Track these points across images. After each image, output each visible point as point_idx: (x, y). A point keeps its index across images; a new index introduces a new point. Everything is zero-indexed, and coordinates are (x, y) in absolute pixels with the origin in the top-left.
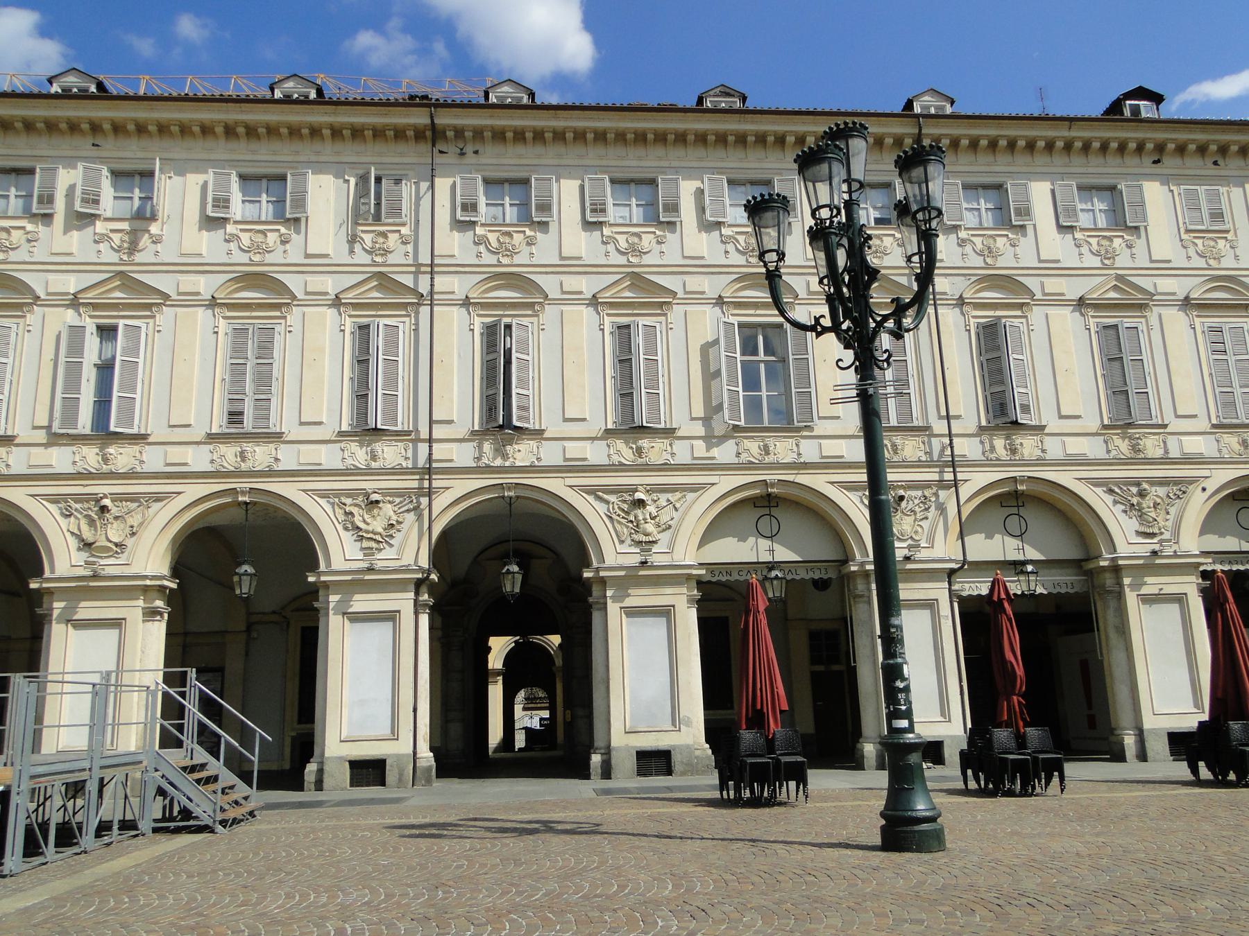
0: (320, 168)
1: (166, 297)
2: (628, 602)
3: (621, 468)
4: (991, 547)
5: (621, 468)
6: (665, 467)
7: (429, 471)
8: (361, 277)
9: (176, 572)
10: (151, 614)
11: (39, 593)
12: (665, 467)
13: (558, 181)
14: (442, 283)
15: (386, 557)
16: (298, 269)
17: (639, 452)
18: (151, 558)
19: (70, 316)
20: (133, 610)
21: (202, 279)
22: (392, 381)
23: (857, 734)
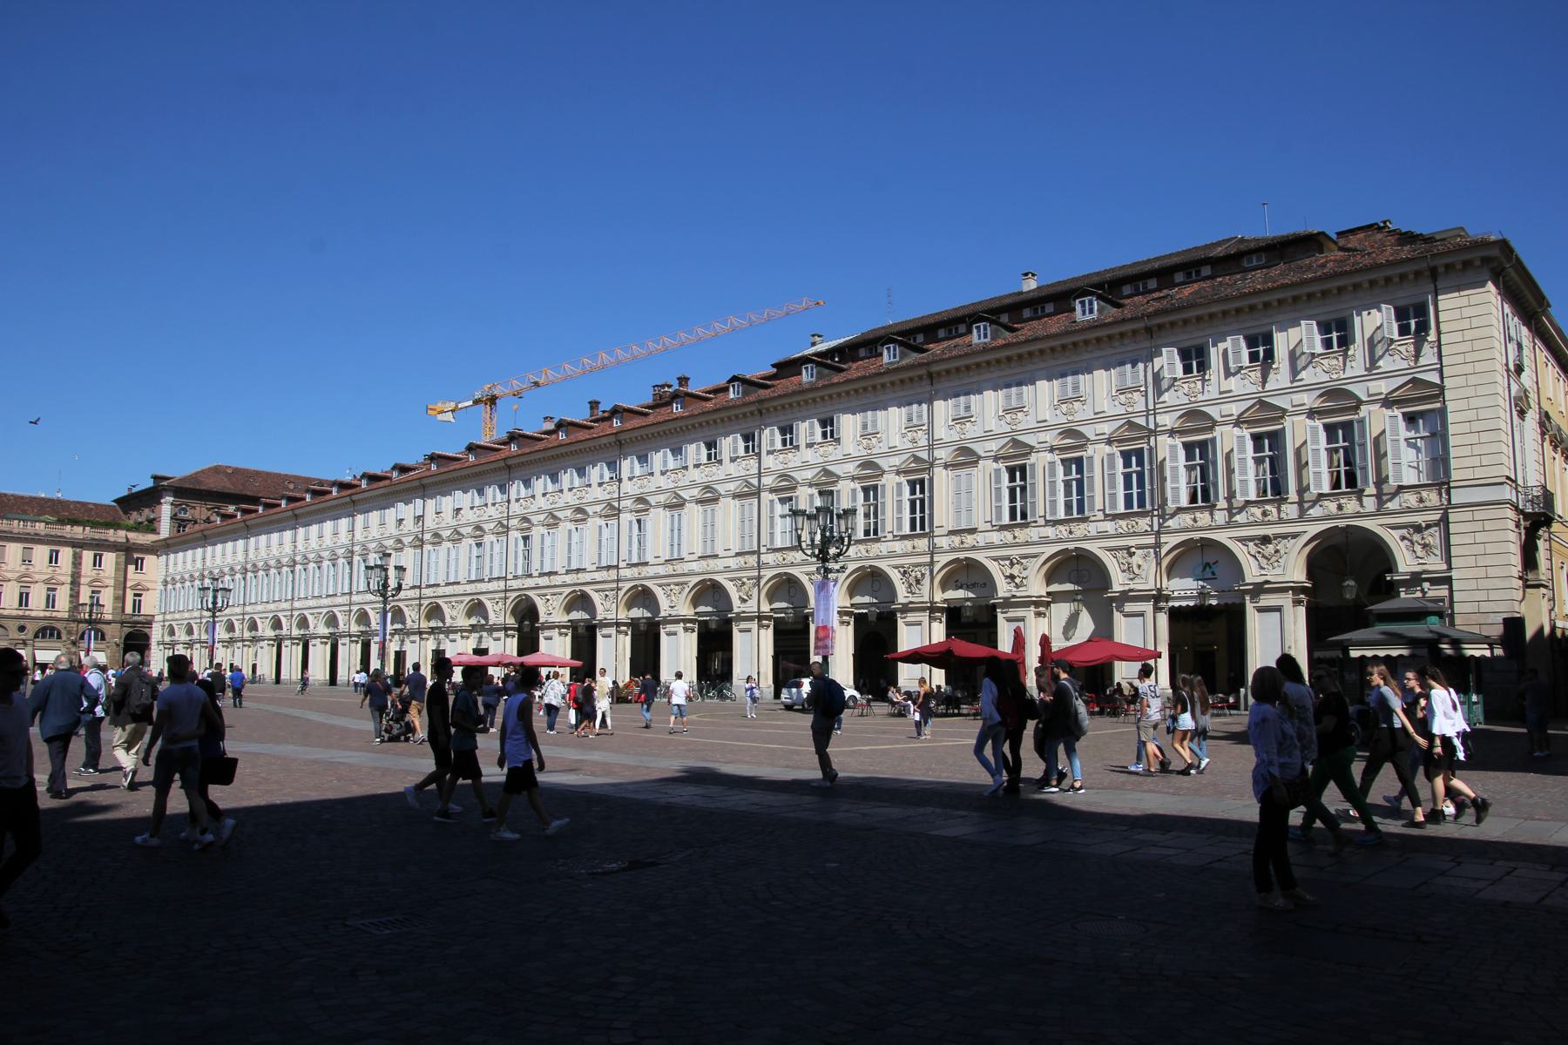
0: (845, 411)
1: (1284, 411)
2: (1263, 603)
3: (1006, 546)
4: (953, 594)
5: (1006, 546)
6: (1027, 544)
7: (618, 581)
8: (1251, 402)
9: (1311, 574)
10: (1297, 603)
11: (1392, 582)
12: (1027, 544)
13: (1359, 314)
14: (623, 504)
15: (1138, 585)
16: (1213, 402)
17: (1195, 520)
18: (1296, 572)
19: (1108, 449)
20: (1285, 600)
21: (1233, 406)
22: (1364, 458)
23: (840, 690)
